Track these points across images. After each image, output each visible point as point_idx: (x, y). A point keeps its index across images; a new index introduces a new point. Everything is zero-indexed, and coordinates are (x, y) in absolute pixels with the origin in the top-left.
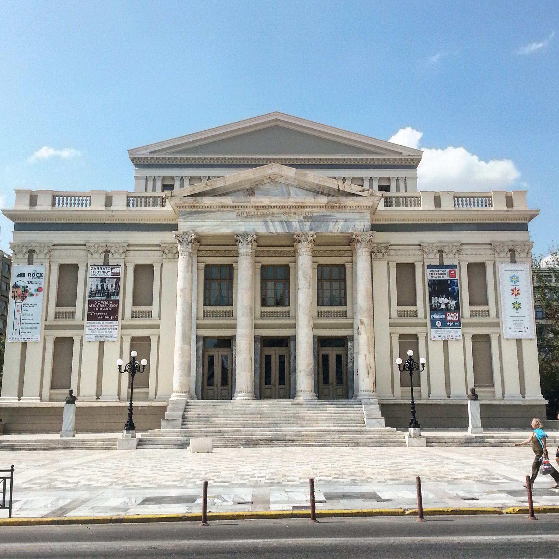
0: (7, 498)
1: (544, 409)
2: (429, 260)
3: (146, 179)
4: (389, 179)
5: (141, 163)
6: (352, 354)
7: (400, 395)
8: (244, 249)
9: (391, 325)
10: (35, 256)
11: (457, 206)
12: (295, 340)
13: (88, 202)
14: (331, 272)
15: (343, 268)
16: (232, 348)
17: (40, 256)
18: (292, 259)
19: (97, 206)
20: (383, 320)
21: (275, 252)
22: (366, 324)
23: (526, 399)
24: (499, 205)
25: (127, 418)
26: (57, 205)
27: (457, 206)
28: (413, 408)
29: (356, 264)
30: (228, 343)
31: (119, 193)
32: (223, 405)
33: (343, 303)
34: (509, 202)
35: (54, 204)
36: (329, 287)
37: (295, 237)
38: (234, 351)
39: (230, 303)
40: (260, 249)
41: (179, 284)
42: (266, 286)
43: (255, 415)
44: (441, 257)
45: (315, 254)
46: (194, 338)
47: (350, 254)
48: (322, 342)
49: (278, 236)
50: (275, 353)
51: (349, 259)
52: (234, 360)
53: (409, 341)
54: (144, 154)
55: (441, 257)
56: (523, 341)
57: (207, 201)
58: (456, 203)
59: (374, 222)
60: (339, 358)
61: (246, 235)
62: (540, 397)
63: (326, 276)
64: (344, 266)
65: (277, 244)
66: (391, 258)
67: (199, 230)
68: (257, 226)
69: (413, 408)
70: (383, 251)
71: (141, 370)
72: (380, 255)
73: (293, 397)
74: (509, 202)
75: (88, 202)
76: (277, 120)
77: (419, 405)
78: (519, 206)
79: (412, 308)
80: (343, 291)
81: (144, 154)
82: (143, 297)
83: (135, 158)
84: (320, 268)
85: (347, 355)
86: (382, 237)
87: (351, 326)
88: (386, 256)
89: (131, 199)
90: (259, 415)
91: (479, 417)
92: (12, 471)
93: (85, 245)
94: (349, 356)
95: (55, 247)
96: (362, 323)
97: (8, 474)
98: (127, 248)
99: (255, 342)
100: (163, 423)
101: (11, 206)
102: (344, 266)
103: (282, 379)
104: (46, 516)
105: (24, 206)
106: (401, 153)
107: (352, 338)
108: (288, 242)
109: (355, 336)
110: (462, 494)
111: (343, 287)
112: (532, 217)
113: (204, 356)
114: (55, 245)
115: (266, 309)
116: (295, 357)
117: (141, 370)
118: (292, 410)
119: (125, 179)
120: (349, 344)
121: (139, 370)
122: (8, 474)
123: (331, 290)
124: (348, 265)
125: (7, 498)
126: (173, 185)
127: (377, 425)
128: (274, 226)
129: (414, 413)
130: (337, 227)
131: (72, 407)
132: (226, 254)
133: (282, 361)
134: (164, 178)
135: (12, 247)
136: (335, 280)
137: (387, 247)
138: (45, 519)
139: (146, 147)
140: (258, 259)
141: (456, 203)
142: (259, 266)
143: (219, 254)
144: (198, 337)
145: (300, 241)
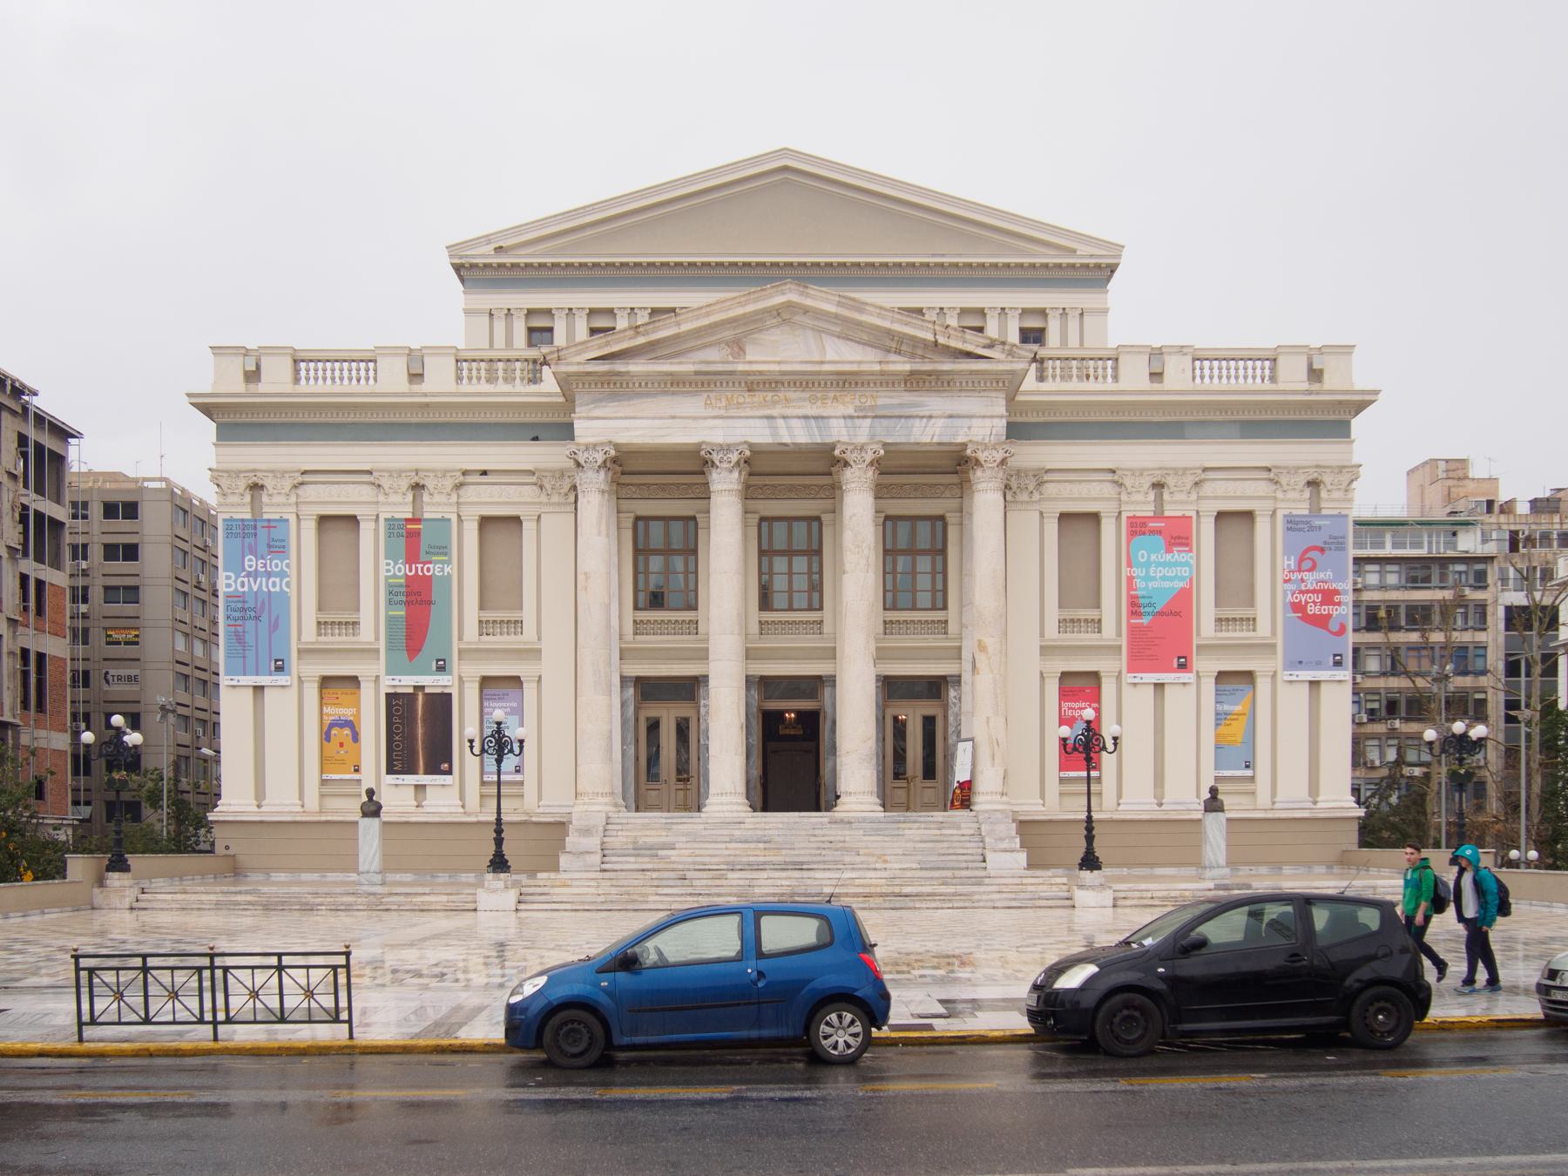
0: (343, 1003)
1: (1355, 826)
2: (1132, 507)
3: (491, 315)
4: (1042, 313)
5: (468, 272)
6: (957, 715)
7: (1056, 801)
8: (725, 486)
9: (1046, 650)
10: (426, 498)
11: (1198, 380)
12: (834, 686)
13: (371, 373)
14: (667, 534)
15: (939, 524)
16: (698, 703)
17: (437, 498)
18: (827, 504)
19: (391, 382)
20: (1027, 644)
21: (792, 488)
22: (990, 649)
23: (1319, 805)
24: (1293, 378)
25: (492, 848)
26: (303, 381)
27: (1198, 380)
28: (499, 831)
29: (971, 514)
30: (689, 689)
31: (439, 351)
32: (686, 823)
33: (816, 604)
34: (1315, 374)
35: (297, 380)
36: (785, 569)
37: (837, 452)
38: (703, 711)
39: (693, 607)
40: (756, 480)
41: (579, 557)
42: (647, 564)
43: (752, 845)
44: (1159, 500)
45: (880, 492)
46: (616, 681)
47: (957, 491)
48: (891, 688)
49: (798, 452)
50: (913, 714)
51: (954, 503)
52: (702, 727)
53: (1080, 686)
54: (481, 256)
55: (1159, 500)
56: (1167, 688)
57: (636, 367)
58: (1198, 372)
59: (1013, 419)
60: (929, 722)
61: (726, 448)
62: (1350, 801)
63: (780, 542)
64: (942, 518)
65: (779, 469)
66: (1045, 506)
67: (622, 439)
68: (756, 432)
69: (499, 831)
70: (1031, 488)
71: (517, 750)
72: (1024, 497)
73: (830, 807)
74: (1315, 374)
75: (371, 373)
76: (786, 169)
77: (1100, 821)
78: (1331, 381)
79: (1090, 614)
80: (939, 577)
81: (484, 254)
82: (500, 592)
83: (462, 266)
84: (641, 524)
85: (946, 717)
86: (1034, 454)
87: (957, 654)
88: (1036, 496)
89: (303, 365)
90: (761, 845)
91: (1223, 847)
92: (348, 954)
93: (370, 472)
94: (951, 719)
95: (307, 478)
96: (982, 647)
97: (342, 960)
98: (1203, 476)
99: (748, 689)
100: (564, 860)
101: (205, 384)
102: (942, 518)
103: (683, 772)
104: (417, 1036)
105: (232, 385)
106: (1074, 251)
107: (957, 680)
108: (820, 466)
109: (966, 677)
110: (851, 411)
111: (939, 568)
112: (1360, 407)
113: (637, 720)
114: (304, 473)
115: (769, 616)
116: (834, 722)
117: (517, 750)
118: (837, 833)
119: (444, 318)
120: (952, 693)
121: (511, 751)
122: (342, 960)
123: (790, 573)
124: (952, 519)
125: (343, 1003)
126: (1042, 331)
127: (1009, 860)
128: (789, 428)
129: (1090, 838)
130: (929, 431)
131: (374, 823)
132: (684, 492)
133: (682, 730)
134: (530, 313)
135: (217, 475)
136: (924, 552)
137: (1040, 477)
138: (422, 1042)
139: (488, 239)
140: (752, 504)
141: (1198, 372)
142: (629, 523)
143: (664, 492)
144: (624, 679)
145: (846, 464)
